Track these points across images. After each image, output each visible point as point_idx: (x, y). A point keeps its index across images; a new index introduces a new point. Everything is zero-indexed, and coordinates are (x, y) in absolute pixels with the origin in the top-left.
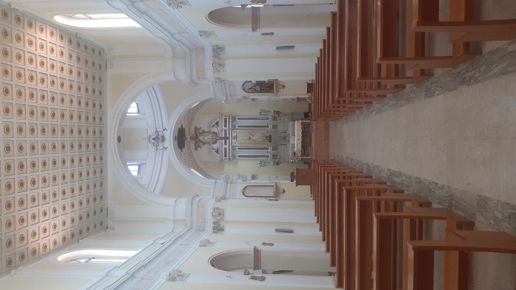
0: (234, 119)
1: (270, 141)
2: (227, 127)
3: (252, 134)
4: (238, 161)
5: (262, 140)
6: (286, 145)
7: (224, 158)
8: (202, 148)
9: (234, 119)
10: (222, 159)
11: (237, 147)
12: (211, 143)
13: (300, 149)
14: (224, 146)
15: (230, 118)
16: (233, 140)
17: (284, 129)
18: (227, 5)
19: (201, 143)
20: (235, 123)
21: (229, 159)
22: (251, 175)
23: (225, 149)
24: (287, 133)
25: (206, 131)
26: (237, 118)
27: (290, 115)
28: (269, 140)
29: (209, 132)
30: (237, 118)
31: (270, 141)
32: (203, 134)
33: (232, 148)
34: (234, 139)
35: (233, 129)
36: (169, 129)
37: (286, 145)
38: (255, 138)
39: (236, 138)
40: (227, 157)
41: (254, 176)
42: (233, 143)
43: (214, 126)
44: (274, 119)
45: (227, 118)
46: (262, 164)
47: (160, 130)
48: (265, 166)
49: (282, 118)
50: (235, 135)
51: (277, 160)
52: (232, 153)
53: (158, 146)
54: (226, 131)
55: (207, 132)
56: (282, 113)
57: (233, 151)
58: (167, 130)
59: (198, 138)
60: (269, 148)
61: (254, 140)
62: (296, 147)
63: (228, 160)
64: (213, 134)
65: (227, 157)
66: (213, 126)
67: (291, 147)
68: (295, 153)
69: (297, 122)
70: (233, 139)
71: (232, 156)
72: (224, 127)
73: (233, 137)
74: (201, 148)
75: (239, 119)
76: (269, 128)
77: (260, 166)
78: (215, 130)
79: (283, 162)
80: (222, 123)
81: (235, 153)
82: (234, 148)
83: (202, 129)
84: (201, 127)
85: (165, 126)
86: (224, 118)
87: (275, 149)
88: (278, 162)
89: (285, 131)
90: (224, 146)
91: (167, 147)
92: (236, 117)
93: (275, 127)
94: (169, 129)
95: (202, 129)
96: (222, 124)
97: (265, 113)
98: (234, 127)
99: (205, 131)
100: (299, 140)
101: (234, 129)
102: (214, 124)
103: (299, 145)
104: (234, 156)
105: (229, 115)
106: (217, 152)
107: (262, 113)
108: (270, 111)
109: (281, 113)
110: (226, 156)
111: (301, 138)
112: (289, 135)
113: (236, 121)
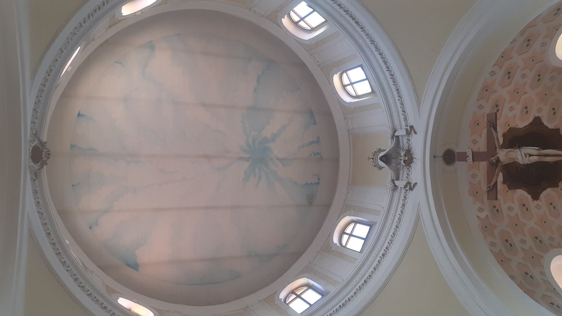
18: (478, 151)
36: (420, 127)
47: (401, 132)
53: (398, 179)
58: (415, 133)
85: (411, 122)
90: (366, 267)
91: (416, 184)
94: (420, 127)
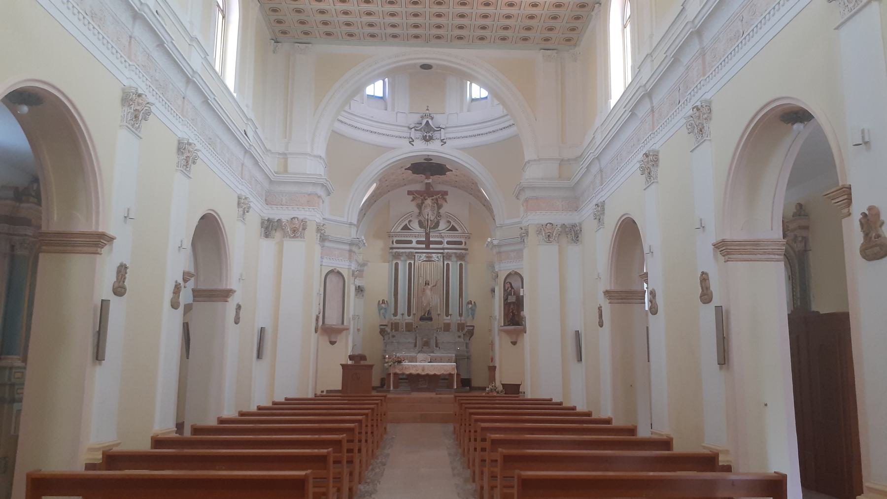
1: (422, 319)
2: (446, 246)
4: (389, 262)
6: (415, 346)
7: (395, 239)
9: (461, 257)
11: (412, 262)
12: (421, 218)
14: (414, 240)
15: (463, 251)
16: (425, 255)
19: (420, 202)
20: (454, 258)
21: (392, 248)
23: (410, 242)
24: (435, 348)
25: (442, 211)
26: (463, 263)
28: (424, 316)
29: (439, 215)
30: (463, 263)
33: (412, 253)
34: (427, 257)
35: (444, 255)
37: (415, 346)
38: (428, 292)
40: (395, 245)
41: (362, 291)
42: (419, 255)
43: (449, 224)
45: (463, 246)
46: (383, 305)
49: (462, 340)
54: (441, 243)
55: (440, 211)
60: (410, 317)
61: (424, 290)
62: (412, 365)
63: (391, 246)
65: (395, 245)
66: (449, 222)
67: (410, 356)
68: (400, 362)
70: (427, 255)
71: (397, 254)
72: (446, 240)
73: (429, 255)
75: (461, 265)
76: (445, 317)
78: (443, 225)
80: (455, 237)
81: (402, 259)
84: (447, 201)
87: (409, 327)
88: (386, 333)
90: (414, 240)
93: (447, 327)
97: (470, 310)
98: (447, 257)
100: (423, 370)
101: (443, 257)
103: (414, 369)
104: (397, 256)
106: (406, 228)
108: (473, 319)
110: (398, 242)
113: (457, 261)
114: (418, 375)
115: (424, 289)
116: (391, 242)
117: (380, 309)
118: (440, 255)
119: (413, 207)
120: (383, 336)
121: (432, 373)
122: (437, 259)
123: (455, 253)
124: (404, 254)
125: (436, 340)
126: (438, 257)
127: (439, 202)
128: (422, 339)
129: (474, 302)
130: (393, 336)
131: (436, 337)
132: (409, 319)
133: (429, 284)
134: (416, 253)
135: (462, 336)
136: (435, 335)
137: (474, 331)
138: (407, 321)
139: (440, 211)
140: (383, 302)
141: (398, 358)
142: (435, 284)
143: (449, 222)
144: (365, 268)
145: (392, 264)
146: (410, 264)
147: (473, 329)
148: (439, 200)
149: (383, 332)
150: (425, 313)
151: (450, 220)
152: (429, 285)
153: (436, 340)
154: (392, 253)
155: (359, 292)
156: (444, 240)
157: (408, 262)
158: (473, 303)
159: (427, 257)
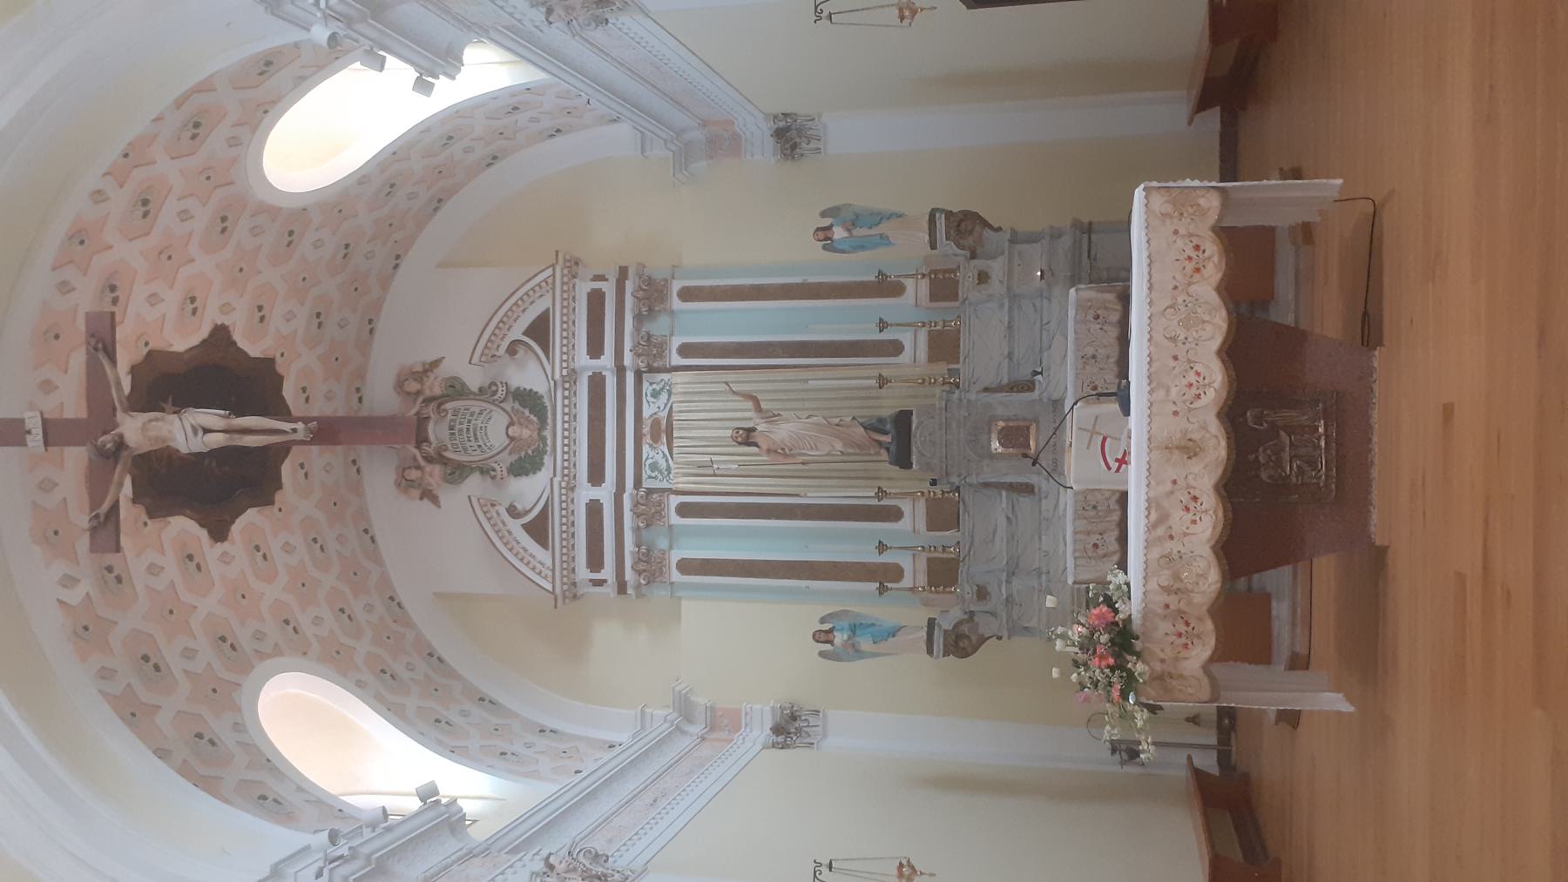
0: (653, 296)
1: (902, 459)
2: (607, 361)
3: (764, 405)
4: (680, 598)
5: (839, 446)
6: (1028, 489)
7: (583, 573)
8: (442, 500)
9: (653, 296)
10: (574, 584)
11: (675, 501)
12: (501, 468)
13: (1206, 578)
14: (586, 493)
15: (629, 286)
16: (646, 449)
17: (1010, 356)
19: (437, 469)
20: (658, 327)
21: (622, 587)
22: (773, 709)
23: (594, 509)
24: (1036, 393)
25: (474, 379)
26: (676, 286)
27: (1066, 241)
28: (893, 448)
29: (486, 393)
30: (676, 286)
31: (902, 459)
32: (448, 406)
33: (636, 504)
34: (656, 438)
35: (642, 366)
37: (1028, 489)
38: (783, 432)
39: (664, 431)
40: (608, 573)
41: (794, 717)
42: (646, 472)
43: (521, 351)
44: (943, 287)
45: (608, 288)
46: (839, 638)
48: (857, 653)
49: (997, 267)
50: (664, 414)
51: (956, 614)
52: (638, 545)
54: (597, 383)
55: (475, 389)
56: (999, 229)
57: (648, 526)
59: (116, 426)
60: (905, 507)
61: (778, 451)
62: (1148, 545)
63: (610, 590)
64: (517, 405)
65: (608, 573)
66: (512, 350)
67: (1077, 517)
68: (1123, 639)
69: (1158, 202)
70: (647, 439)
71: (641, 566)
72: (582, 359)
73: (646, 430)
74: (434, 499)
75: (687, 294)
76: (906, 357)
77: (822, 654)
78: (530, 375)
79: (1005, 634)
80: (569, 323)
81: (662, 543)
82: (650, 509)
83: (445, 370)
84: (430, 358)
86: (584, 288)
87: (943, 515)
88: (965, 629)
89: (1024, 373)
90: (586, 493)
92: (666, 283)
93: (944, 346)
95: (445, 370)
96: (569, 337)
97: (857, 232)
98: (652, 359)
99: (463, 385)
100: (1190, 449)
101: (651, 370)
102: (517, 333)
103: (1179, 520)
104: (651, 567)
105: (623, 273)
106: (539, 529)
107: (839, 233)
108: (900, 216)
109: (986, 224)
110: (595, 562)
111: (1215, 428)
112: (1057, 404)
113: (672, 313)
114: (1233, 486)
115: (769, 451)
116: (598, 589)
117: (853, 652)
118: (645, 385)
119: (457, 499)
120: (983, 640)
121: (1215, 376)
122: (664, 396)
123: (639, 318)
124: (644, 533)
125: (999, 389)
126: (655, 394)
127: (437, 391)
128: (993, 457)
129: (824, 214)
130: (982, 594)
131: (986, 390)
132: (914, 517)
133: (750, 430)
134: (638, 483)
135: (979, 263)
136: (973, 397)
137: (955, 210)
138: (922, 524)
139: (475, 389)
140: (824, 637)
141: (1088, 644)
142: (750, 404)
143: (512, 350)
144: (701, 700)
145: (685, 586)
146: (684, 510)
147: (949, 214)
148: (428, 393)
149: (960, 643)
150: (880, 443)
151: (505, 344)
152: (753, 430)
153: (999, 389)
154: (638, 587)
155: (799, 731)
156: (585, 368)
157: (675, 519)
158: (826, 222)
159: (656, 438)
